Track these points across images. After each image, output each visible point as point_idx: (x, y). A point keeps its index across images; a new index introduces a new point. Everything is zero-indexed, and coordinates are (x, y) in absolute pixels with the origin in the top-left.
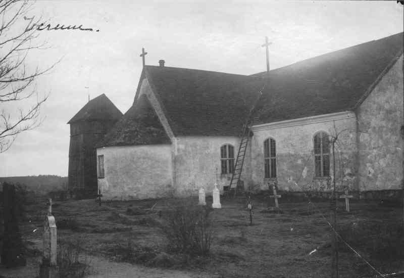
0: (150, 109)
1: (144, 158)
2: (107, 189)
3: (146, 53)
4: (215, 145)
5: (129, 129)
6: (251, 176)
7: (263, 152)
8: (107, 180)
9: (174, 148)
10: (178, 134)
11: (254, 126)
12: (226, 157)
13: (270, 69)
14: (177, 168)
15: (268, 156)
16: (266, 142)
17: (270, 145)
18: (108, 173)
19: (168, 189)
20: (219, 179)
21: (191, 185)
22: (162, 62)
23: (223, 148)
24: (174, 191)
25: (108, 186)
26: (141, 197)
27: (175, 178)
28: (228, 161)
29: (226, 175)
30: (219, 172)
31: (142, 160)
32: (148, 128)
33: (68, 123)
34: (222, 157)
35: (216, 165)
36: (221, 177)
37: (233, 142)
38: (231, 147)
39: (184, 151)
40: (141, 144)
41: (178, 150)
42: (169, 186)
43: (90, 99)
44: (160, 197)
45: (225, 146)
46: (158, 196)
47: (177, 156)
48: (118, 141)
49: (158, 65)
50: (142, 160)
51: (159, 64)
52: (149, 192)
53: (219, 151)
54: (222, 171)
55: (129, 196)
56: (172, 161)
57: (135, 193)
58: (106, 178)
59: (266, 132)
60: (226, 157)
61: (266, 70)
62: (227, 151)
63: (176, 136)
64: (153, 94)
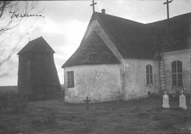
0: (100, 40)
1: (104, 73)
2: (76, 95)
3: (91, 5)
4: (145, 63)
5: (91, 53)
6: (67, 96)
7: (171, 70)
8: (77, 88)
9: (123, 67)
10: (126, 56)
11: (164, 53)
12: (148, 73)
13: (170, 17)
14: (125, 79)
15: (176, 72)
16: (174, 64)
17: (177, 66)
18: (78, 84)
19: (118, 94)
20: (146, 87)
21: (132, 91)
22: (103, 10)
23: (147, 67)
24: (122, 96)
25: (77, 92)
26: (102, 101)
27: (123, 87)
28: (149, 75)
29: (149, 85)
30: (146, 82)
31: (102, 74)
32: (103, 53)
33: (17, 54)
34: (147, 73)
35: (144, 78)
36: (147, 86)
37: (150, 63)
38: (151, 66)
39: (128, 68)
40: (102, 64)
41: (126, 67)
42: (119, 92)
43: (30, 41)
44: (114, 100)
45: (175, 62)
46: (113, 99)
47: (125, 72)
48: (86, 61)
49: (101, 12)
50: (102, 74)
51: (101, 11)
52: (107, 97)
53: (145, 69)
54: (147, 82)
55: (94, 100)
56: (121, 76)
57: (98, 97)
58: (75, 87)
59: (172, 57)
60: (148, 73)
61: (167, 18)
62: (149, 69)
63: (125, 58)
64: (102, 30)
